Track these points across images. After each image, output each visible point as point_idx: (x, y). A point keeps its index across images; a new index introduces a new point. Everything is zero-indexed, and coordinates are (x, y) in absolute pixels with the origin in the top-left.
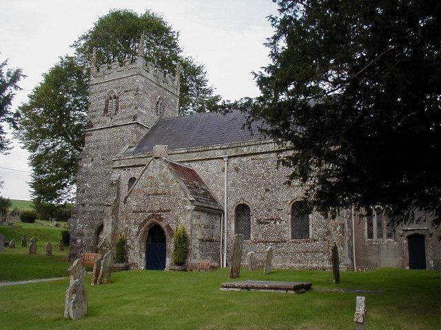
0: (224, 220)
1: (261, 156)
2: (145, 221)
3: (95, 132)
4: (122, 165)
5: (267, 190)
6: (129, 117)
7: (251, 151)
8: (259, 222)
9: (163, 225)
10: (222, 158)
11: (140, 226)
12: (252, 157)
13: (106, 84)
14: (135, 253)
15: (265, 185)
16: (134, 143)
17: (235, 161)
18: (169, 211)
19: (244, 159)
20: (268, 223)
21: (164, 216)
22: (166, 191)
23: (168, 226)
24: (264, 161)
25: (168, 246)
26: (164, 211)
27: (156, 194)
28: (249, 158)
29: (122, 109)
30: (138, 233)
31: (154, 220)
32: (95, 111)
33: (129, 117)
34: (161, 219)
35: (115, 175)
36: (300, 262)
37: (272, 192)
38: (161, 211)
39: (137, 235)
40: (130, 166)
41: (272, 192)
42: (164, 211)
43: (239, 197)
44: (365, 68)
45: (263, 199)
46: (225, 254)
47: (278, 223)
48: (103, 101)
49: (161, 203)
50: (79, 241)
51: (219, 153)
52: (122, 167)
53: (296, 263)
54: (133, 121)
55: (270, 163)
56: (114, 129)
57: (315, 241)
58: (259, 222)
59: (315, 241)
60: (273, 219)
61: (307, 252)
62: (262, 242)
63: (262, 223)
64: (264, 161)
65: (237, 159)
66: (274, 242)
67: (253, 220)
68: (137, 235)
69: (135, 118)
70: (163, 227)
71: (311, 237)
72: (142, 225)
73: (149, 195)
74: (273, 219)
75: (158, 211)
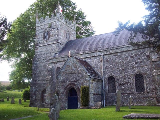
1: (119, 54)
3: (39, 48)
4: (53, 62)
5: (123, 70)
6: (55, 40)
9: (76, 88)
11: (64, 89)
12: (115, 54)
14: (62, 102)
15: (122, 67)
16: (58, 51)
17: (106, 57)
18: (78, 81)
19: (111, 56)
20: (124, 85)
21: (76, 84)
22: (77, 72)
24: (120, 56)
26: (76, 81)
27: (72, 73)
28: (113, 55)
31: (71, 85)
33: (55, 40)
34: (75, 85)
35: (50, 67)
36: (141, 103)
37: (125, 70)
38: (74, 81)
41: (125, 70)
42: (76, 81)
43: (109, 73)
45: (121, 74)
46: (104, 100)
47: (129, 85)
48: (42, 34)
49: (74, 77)
50: (34, 97)
52: (53, 63)
53: (139, 103)
54: (57, 42)
55: (123, 57)
56: (48, 46)
57: (148, 92)
58: (120, 84)
60: (126, 83)
61: (144, 98)
63: (121, 85)
65: (107, 56)
69: (57, 40)
73: (68, 74)
74: (126, 83)
75: (73, 81)
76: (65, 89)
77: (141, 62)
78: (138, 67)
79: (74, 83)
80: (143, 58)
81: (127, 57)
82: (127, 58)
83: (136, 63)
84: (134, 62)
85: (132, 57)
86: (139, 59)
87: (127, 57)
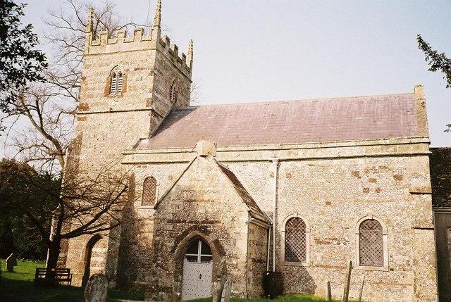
0: (272, 233)
2: (185, 234)
5: (328, 203)
7: (308, 156)
8: (318, 242)
10: (271, 161)
12: (310, 162)
13: (107, 57)
18: (412, 193)
19: (299, 164)
20: (329, 243)
23: (217, 242)
25: (109, 256)
29: (131, 90)
30: (174, 249)
31: (198, 233)
32: (92, 89)
39: (173, 251)
40: (147, 163)
44: (52, 228)
45: (323, 213)
47: (342, 244)
51: (267, 155)
55: (333, 171)
58: (318, 242)
59: (392, 270)
60: (336, 239)
62: (322, 266)
64: (324, 168)
66: (337, 267)
67: (309, 239)
68: (173, 251)
70: (209, 242)
71: (386, 264)
72: (178, 239)
74: (336, 239)
75: (203, 222)
76: (177, 241)
77: (378, 190)
78: (368, 201)
79: (207, 227)
80: (385, 179)
81: (343, 174)
82: (341, 175)
83: (366, 191)
84: (361, 189)
85: (356, 174)
86: (374, 181)
87: (343, 174)
